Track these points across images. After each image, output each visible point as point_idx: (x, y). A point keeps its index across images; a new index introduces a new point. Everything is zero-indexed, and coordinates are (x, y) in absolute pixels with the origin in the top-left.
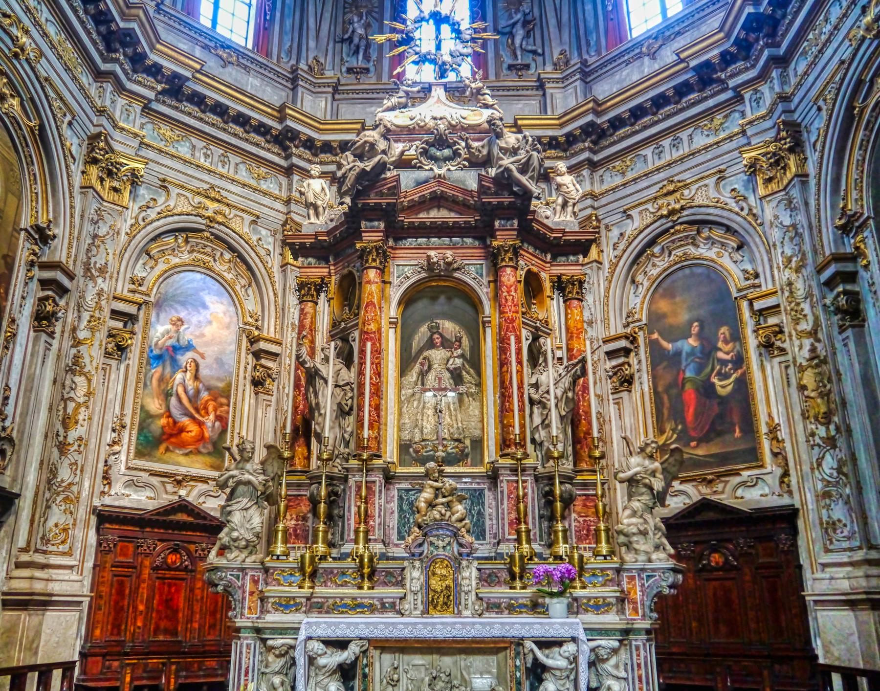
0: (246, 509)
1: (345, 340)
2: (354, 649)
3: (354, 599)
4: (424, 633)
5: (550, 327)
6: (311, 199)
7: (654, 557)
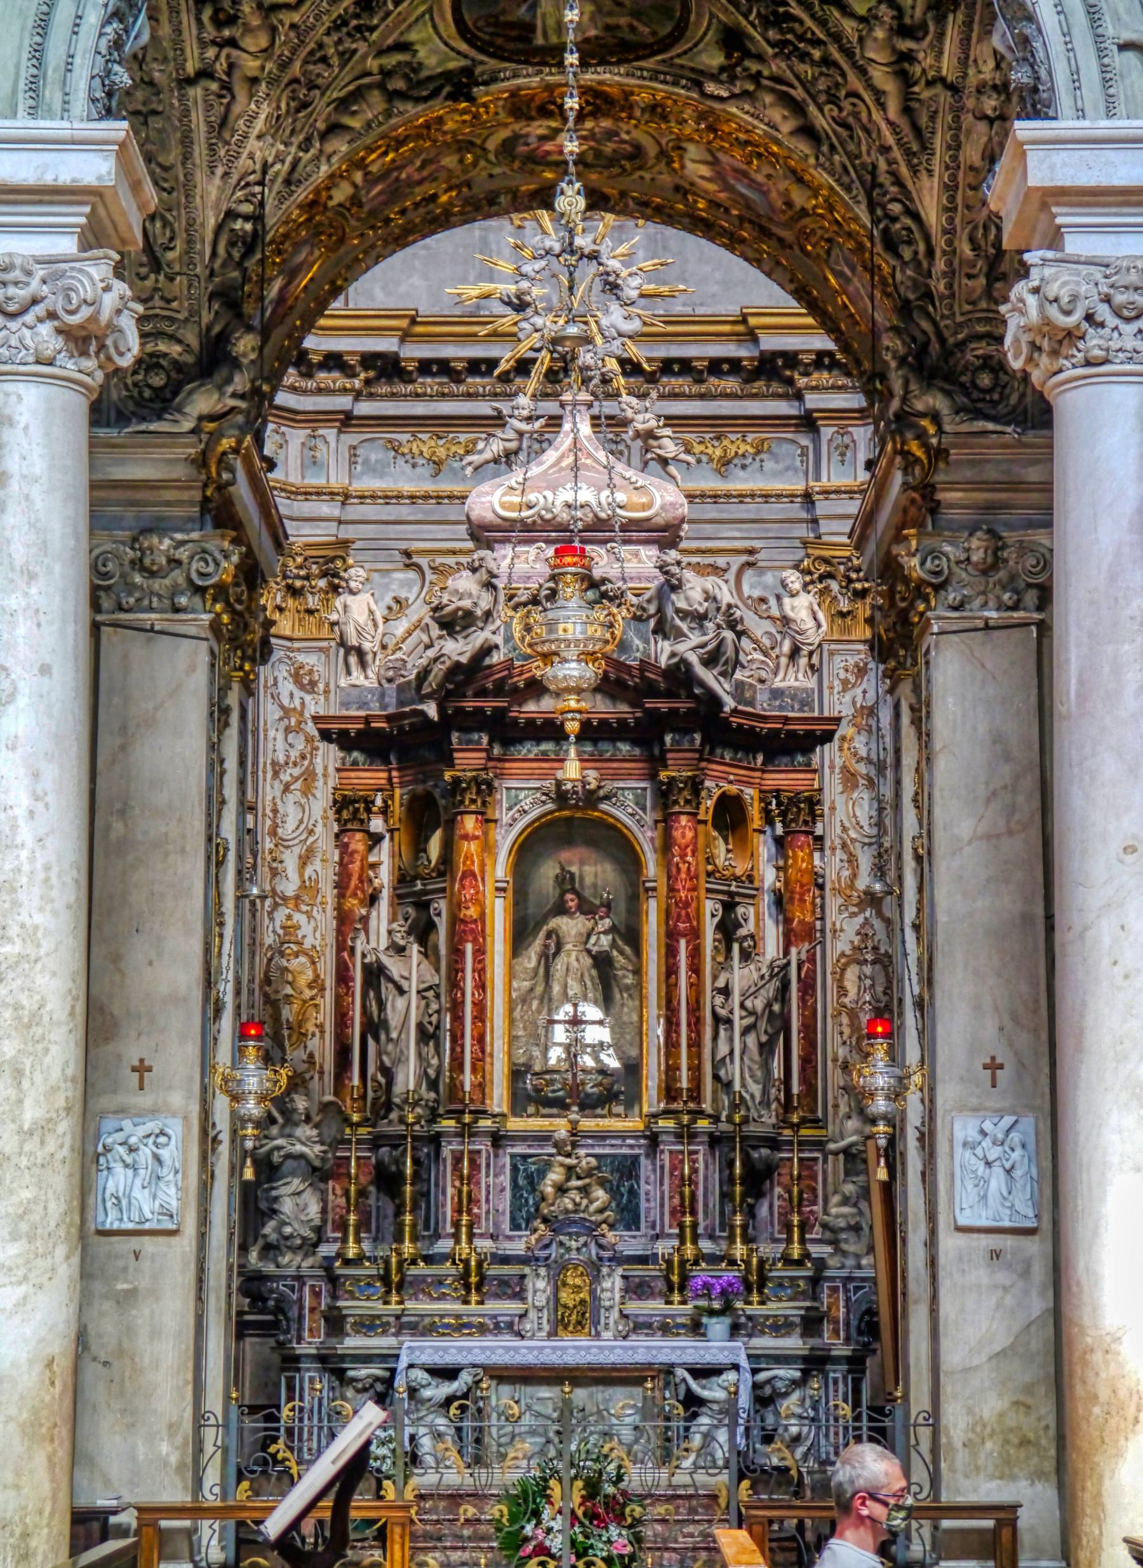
0: (299, 1194)
1: (423, 906)
2: (465, 1378)
3: (458, 1317)
5: (756, 884)
6: (353, 641)
7: (864, 1262)
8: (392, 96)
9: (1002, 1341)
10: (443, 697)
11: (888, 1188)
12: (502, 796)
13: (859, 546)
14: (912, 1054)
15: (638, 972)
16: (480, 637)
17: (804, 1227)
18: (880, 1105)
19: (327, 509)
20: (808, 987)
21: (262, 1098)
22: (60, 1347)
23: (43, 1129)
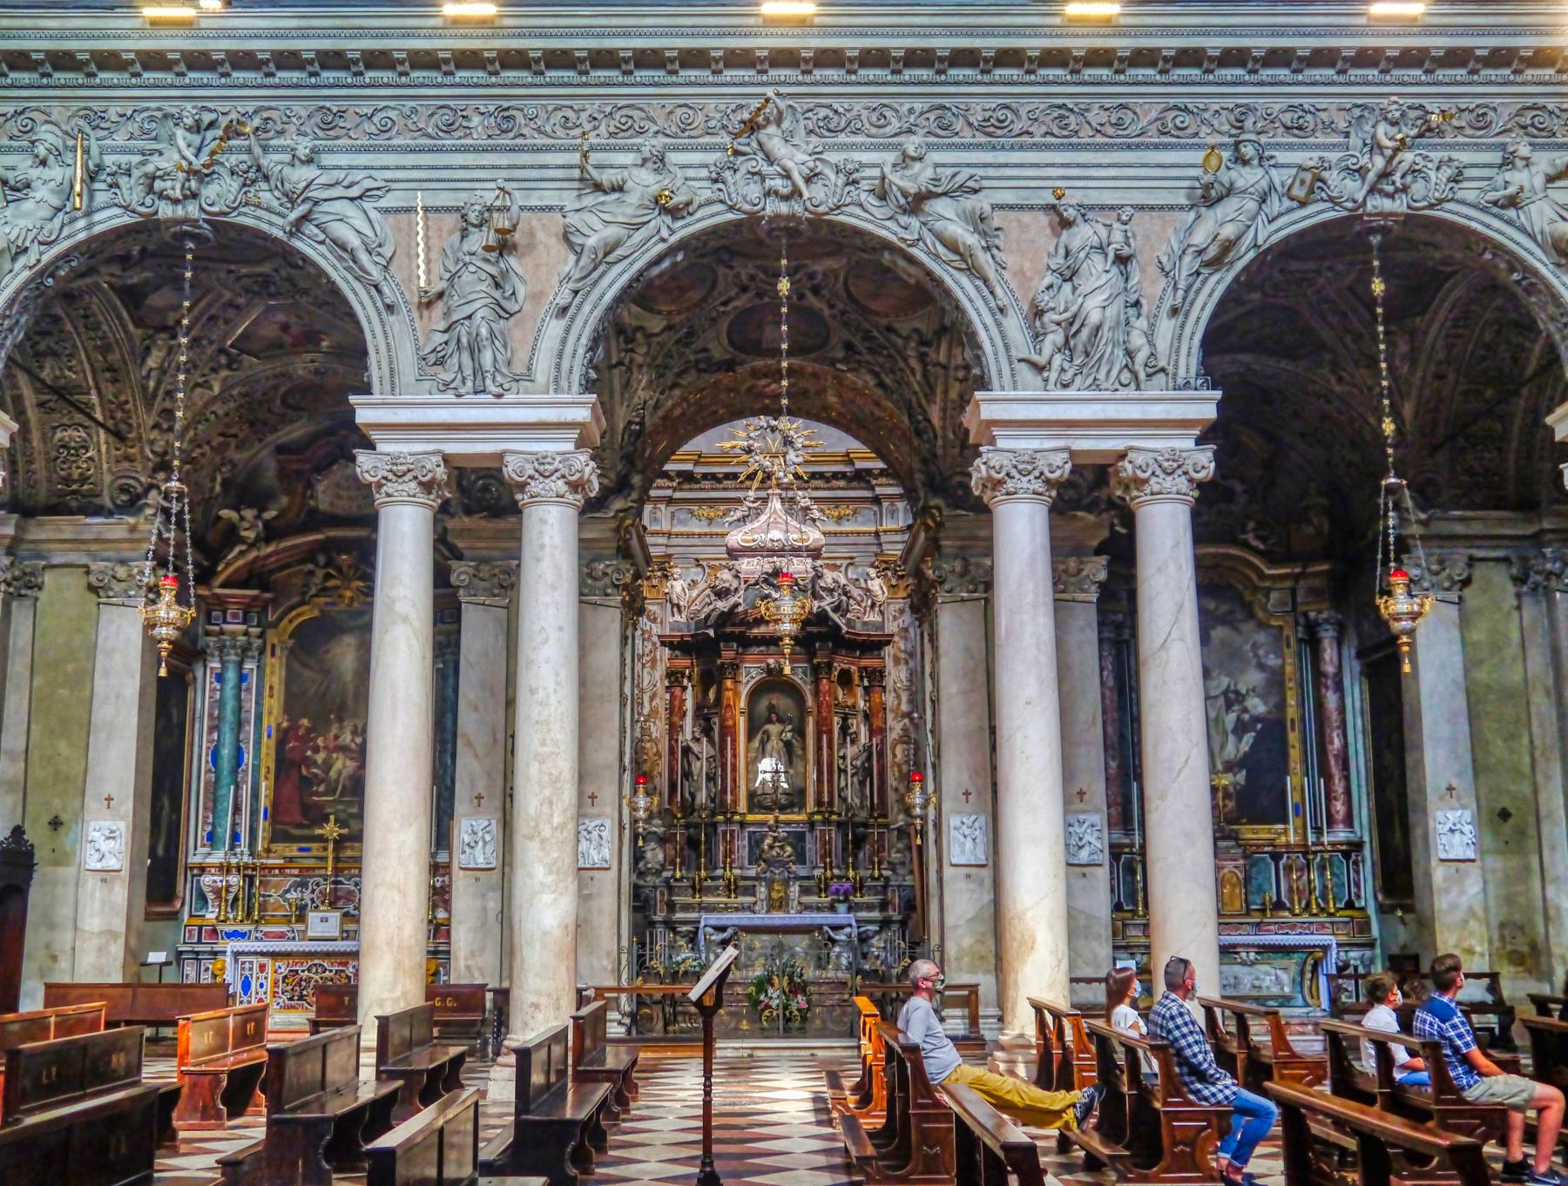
1: (707, 720)
2: (730, 931)
4: (768, 922)
8: (700, 371)
9: (971, 913)
10: (716, 626)
11: (920, 848)
12: (743, 671)
13: (905, 563)
14: (930, 787)
15: (804, 748)
16: (732, 600)
17: (880, 863)
18: (918, 811)
19: (661, 540)
20: (881, 755)
21: (646, 810)
22: (571, 920)
23: (562, 826)
